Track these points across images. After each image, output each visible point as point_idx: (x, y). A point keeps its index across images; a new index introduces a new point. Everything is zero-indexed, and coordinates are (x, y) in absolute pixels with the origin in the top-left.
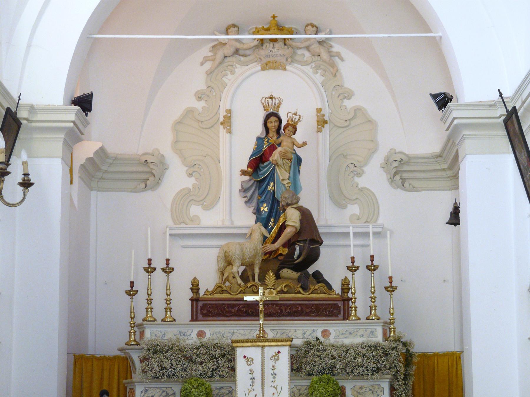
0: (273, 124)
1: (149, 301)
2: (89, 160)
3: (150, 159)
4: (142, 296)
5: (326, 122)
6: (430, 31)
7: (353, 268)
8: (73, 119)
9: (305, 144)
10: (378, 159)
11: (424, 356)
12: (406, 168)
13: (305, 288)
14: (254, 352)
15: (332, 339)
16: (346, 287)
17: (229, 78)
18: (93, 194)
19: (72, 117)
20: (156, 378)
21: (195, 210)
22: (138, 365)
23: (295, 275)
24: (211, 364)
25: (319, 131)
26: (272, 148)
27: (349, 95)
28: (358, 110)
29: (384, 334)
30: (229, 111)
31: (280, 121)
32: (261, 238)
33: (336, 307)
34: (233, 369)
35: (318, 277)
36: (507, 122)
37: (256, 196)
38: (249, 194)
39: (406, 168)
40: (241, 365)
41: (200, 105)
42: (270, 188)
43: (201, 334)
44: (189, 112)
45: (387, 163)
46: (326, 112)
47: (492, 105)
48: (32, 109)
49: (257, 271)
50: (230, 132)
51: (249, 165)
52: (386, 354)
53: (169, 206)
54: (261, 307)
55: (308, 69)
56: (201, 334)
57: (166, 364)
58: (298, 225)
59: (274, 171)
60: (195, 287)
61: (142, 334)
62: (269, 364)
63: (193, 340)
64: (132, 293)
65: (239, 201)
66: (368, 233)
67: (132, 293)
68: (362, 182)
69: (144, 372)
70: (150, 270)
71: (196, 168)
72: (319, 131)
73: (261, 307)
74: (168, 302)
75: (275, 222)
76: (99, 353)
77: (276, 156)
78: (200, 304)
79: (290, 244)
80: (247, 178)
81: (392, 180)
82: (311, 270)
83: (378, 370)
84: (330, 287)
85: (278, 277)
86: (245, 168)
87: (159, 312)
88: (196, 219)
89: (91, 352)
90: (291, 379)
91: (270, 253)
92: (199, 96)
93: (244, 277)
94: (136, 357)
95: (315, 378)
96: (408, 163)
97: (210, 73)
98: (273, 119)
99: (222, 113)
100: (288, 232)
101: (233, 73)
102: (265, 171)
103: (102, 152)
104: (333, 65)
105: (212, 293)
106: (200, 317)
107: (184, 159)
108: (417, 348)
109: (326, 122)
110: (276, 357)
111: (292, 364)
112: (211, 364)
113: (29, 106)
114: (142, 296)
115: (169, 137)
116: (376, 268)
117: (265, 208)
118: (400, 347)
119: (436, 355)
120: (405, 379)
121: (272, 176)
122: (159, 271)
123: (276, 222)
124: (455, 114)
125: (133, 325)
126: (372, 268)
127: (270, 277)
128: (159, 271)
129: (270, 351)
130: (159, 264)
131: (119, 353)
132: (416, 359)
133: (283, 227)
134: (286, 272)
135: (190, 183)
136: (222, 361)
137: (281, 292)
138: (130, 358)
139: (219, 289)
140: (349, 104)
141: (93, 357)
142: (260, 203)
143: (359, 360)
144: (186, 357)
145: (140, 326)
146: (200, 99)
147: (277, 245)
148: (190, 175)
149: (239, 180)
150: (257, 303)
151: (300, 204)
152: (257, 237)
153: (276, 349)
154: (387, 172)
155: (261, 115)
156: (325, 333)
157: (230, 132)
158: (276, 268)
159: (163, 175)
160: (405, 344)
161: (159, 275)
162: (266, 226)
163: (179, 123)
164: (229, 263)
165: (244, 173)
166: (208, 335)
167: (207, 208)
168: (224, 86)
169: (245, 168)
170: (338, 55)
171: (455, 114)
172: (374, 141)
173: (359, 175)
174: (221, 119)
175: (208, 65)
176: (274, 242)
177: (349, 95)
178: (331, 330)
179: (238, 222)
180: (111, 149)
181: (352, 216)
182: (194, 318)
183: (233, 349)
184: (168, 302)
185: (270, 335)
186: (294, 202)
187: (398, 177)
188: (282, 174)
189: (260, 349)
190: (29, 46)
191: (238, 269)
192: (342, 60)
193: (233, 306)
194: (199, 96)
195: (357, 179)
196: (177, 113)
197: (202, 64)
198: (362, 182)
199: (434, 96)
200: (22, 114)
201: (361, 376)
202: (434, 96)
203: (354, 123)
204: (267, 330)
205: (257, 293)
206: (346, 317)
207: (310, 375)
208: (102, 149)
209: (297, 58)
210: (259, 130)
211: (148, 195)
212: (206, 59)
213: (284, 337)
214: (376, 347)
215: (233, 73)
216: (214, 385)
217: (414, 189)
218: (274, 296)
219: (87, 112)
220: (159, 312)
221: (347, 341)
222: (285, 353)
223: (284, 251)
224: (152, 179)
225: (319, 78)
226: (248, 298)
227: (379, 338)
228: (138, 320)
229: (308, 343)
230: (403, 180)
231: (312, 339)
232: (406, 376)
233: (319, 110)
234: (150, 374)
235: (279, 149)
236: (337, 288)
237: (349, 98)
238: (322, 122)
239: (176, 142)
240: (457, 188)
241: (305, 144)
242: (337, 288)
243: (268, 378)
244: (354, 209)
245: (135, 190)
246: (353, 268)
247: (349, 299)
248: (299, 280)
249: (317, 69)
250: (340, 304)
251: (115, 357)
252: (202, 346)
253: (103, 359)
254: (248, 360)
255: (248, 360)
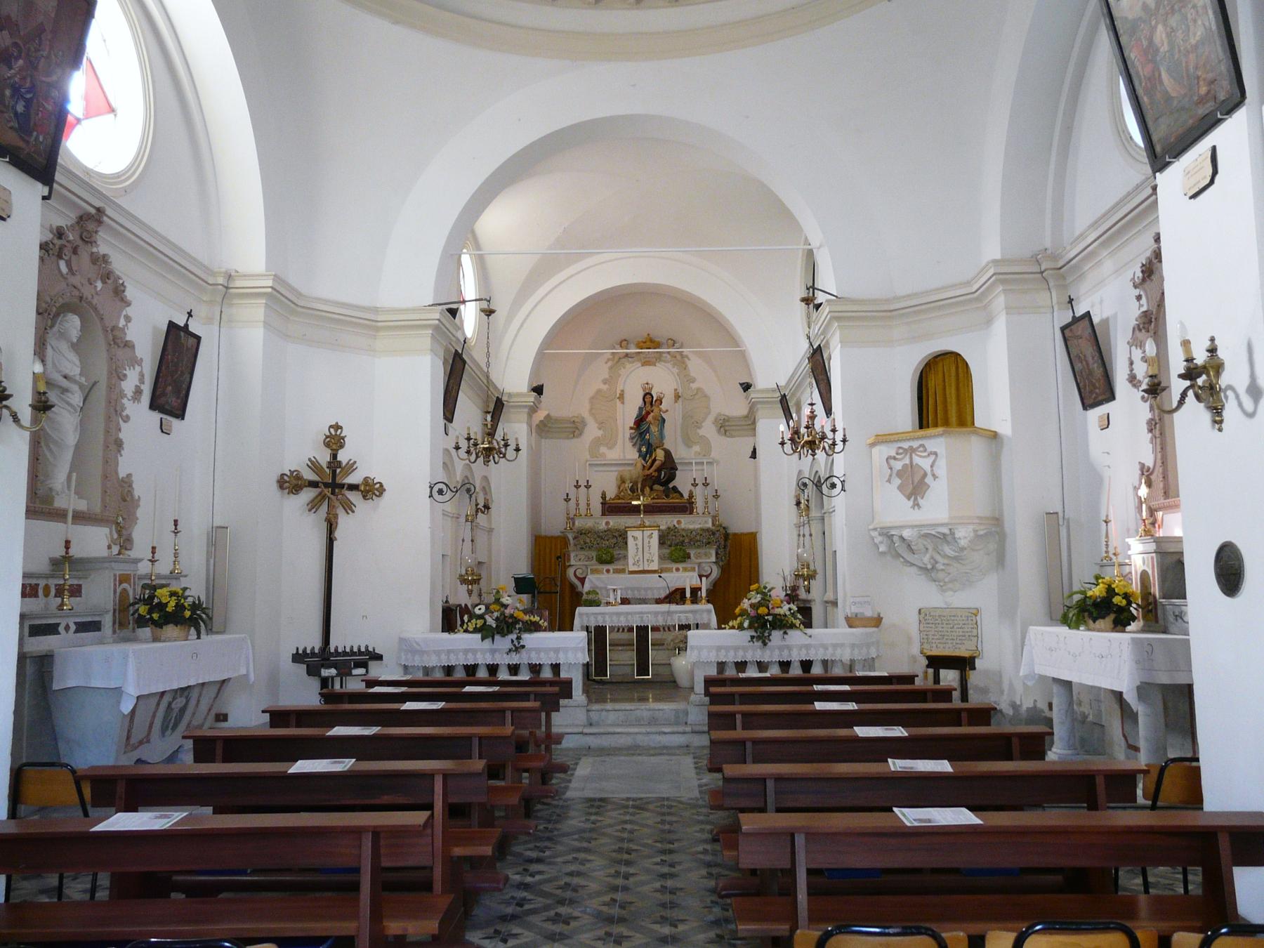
0: (648, 399)
1: (578, 505)
2: (541, 421)
3: (576, 420)
4: (573, 502)
5: (679, 397)
6: (739, 347)
7: (695, 485)
8: (438, 317)
9: (667, 411)
10: (711, 418)
11: (735, 535)
12: (727, 424)
13: (667, 496)
14: (638, 534)
15: (683, 526)
16: (691, 496)
17: (622, 371)
18: (543, 440)
19: (532, 399)
20: (582, 548)
21: (603, 449)
22: (572, 541)
23: (662, 488)
24: (614, 541)
25: (676, 402)
26: (648, 413)
27: (693, 381)
28: (699, 389)
29: (713, 521)
30: (623, 391)
31: (653, 397)
32: (642, 467)
33: (685, 506)
34: (626, 543)
35: (675, 489)
36: (781, 402)
37: (639, 442)
38: (635, 441)
39: (727, 424)
40: (630, 541)
41: (605, 387)
42: (647, 437)
43: (607, 523)
44: (599, 391)
45: (716, 421)
46: (680, 391)
47: (773, 391)
48: (510, 395)
49: (639, 486)
50: (623, 403)
51: (635, 424)
52: (714, 534)
53: (587, 446)
54: (642, 507)
55: (669, 365)
56: (607, 523)
57: (588, 541)
58: (663, 459)
59: (649, 427)
60: (604, 496)
61: (574, 524)
62: (646, 540)
63: (603, 526)
64: (567, 500)
65: (629, 444)
66: (692, 463)
67: (567, 500)
68: (701, 432)
69: (575, 545)
70: (577, 486)
71: (603, 425)
72: (676, 402)
73: (642, 507)
74: (588, 505)
75: (650, 457)
76: (549, 534)
77: (650, 418)
78: (607, 506)
79: (659, 470)
80: (633, 431)
81: (719, 431)
82: (671, 485)
83: (709, 543)
84: (682, 495)
85: (651, 489)
86: (632, 425)
87: (583, 511)
88: (603, 455)
89: (543, 534)
90: (659, 548)
91: (647, 475)
92: (605, 382)
93: (632, 490)
94: (570, 536)
95: (673, 548)
96: (728, 421)
97: (611, 368)
98: (648, 396)
99: (618, 392)
100: (657, 463)
101: (624, 368)
102: (644, 427)
103: (548, 416)
104: (684, 363)
105: (613, 500)
106: (607, 513)
107: (596, 420)
108: (733, 530)
109: (679, 397)
110: (650, 536)
111: (660, 540)
112: (614, 541)
113: (526, 406)
114: (573, 502)
115: (587, 406)
116: (708, 484)
117: (644, 449)
118: (722, 530)
119: (742, 534)
120: (724, 548)
121: (648, 430)
122: (583, 487)
123: (650, 457)
124: (752, 396)
125: (568, 518)
126: (706, 485)
127: (647, 490)
128: (583, 487)
129: (647, 533)
130: (582, 483)
131: (560, 534)
132: (730, 537)
133: (655, 460)
134: (656, 487)
135: (600, 433)
136: (620, 539)
137: (654, 498)
138: (648, 344)
139: (618, 497)
140: (694, 386)
141: (546, 537)
142: (641, 446)
143: (698, 537)
144: (599, 537)
145: (572, 519)
146: (605, 383)
147: (651, 470)
148: (600, 429)
149: (628, 433)
150: (639, 505)
151: (665, 446)
152: (639, 466)
153: (651, 532)
154: (716, 426)
155: (641, 394)
156: (679, 522)
157: (623, 403)
158: (651, 484)
159: (583, 428)
160: (724, 528)
161: (583, 489)
162: (644, 459)
163: (593, 398)
164: (623, 481)
165: (631, 428)
166: (611, 524)
167: (610, 448)
168: (620, 375)
169: (632, 425)
170: (687, 356)
171: (752, 396)
172: (708, 407)
173: (699, 428)
174: (618, 395)
175: (610, 364)
176: (649, 469)
177: (693, 381)
178: (682, 520)
179: (628, 457)
180: (552, 414)
181: (696, 452)
182: (603, 514)
183: (626, 532)
184: (588, 505)
185: (647, 523)
186: (661, 445)
187: (722, 429)
188: (654, 429)
189: (641, 532)
190: (507, 358)
191: (628, 485)
192: (689, 359)
193: (625, 507)
194: (605, 382)
195: (699, 431)
196: (591, 392)
197: (606, 363)
198: (701, 432)
199: (741, 384)
200: (504, 398)
201: (699, 547)
202: (741, 384)
203: (697, 397)
204: (646, 521)
205: (639, 499)
206: (691, 513)
207: (670, 546)
208: (548, 415)
209: (663, 359)
210: (640, 402)
211: (575, 440)
212: (609, 360)
213: (655, 524)
214: (708, 530)
215: (624, 368)
216: (615, 553)
217: (732, 436)
218: (648, 501)
219: (737, 611)
220: (583, 511)
221: (691, 527)
222: (656, 535)
223: (656, 474)
224: (577, 431)
225: (675, 370)
226: (635, 503)
227: (710, 525)
228: (571, 516)
229: (669, 528)
230: (726, 431)
231: (672, 526)
232: (725, 547)
233: (676, 390)
234: (579, 547)
235: (652, 414)
236: (686, 496)
237: (693, 382)
238: (677, 397)
239: (591, 409)
240: (755, 435)
241: (667, 411)
242: (686, 496)
243: (646, 549)
244: (696, 448)
245: (568, 438)
246: (695, 485)
247: (693, 503)
248: (664, 491)
249: (674, 365)
250: (688, 505)
251: (558, 537)
252: (609, 530)
253: (552, 537)
254: (635, 538)
255: (635, 538)
